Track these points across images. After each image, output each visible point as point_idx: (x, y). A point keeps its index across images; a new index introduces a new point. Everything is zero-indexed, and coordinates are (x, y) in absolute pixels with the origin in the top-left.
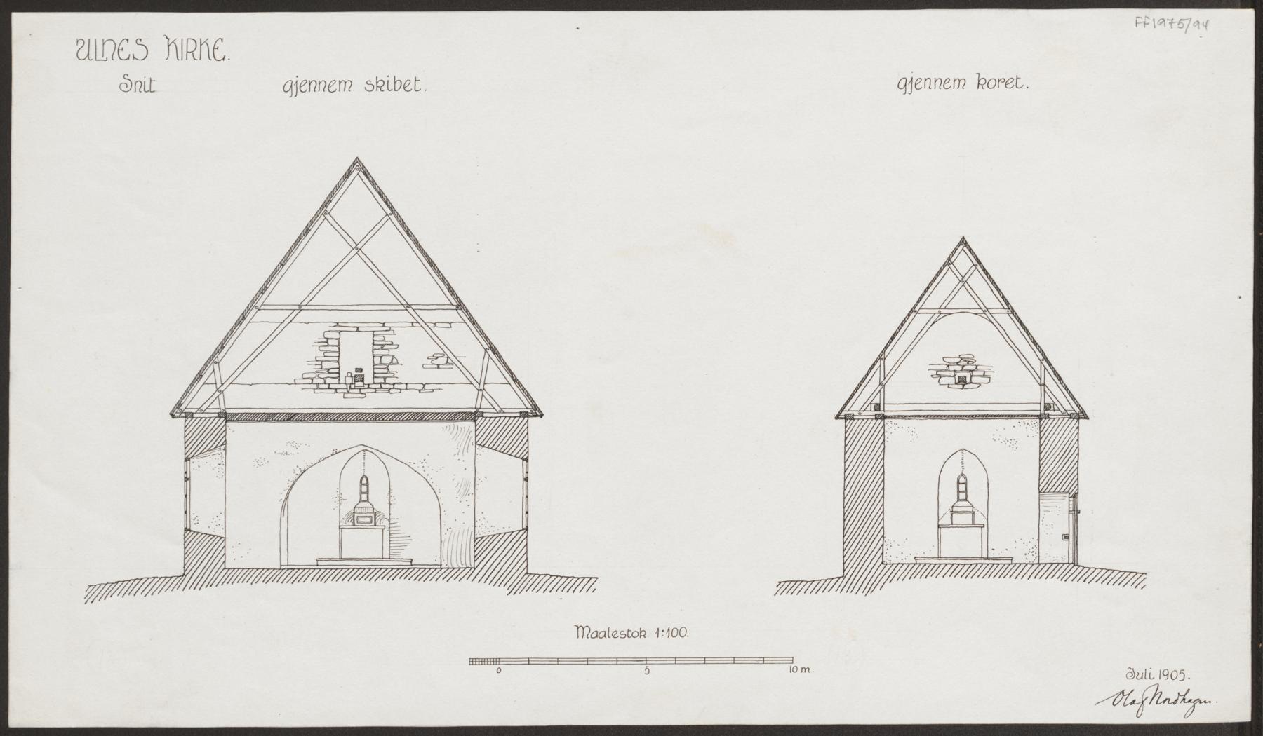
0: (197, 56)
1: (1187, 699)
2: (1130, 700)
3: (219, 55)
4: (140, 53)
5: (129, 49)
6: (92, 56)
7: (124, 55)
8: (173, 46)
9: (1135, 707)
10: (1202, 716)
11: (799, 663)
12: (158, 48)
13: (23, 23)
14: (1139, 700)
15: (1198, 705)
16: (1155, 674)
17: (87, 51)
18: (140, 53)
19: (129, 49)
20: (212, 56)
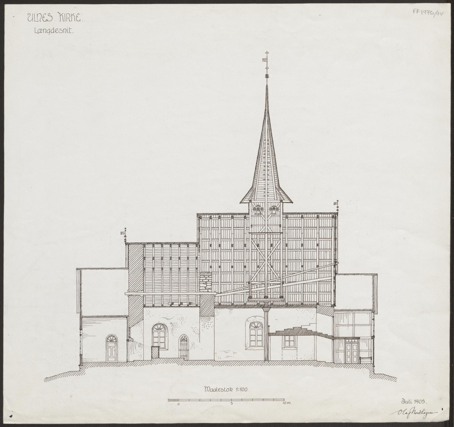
0: (71, 20)
2: (405, 412)
3: (78, 19)
4: (49, 18)
5: (46, 17)
7: (45, 19)
8: (61, 16)
10: (430, 419)
11: (286, 401)
12: (56, 17)
13: (9, 9)
14: (408, 413)
15: (428, 414)
17: (32, 18)
18: (49, 18)
19: (46, 17)
20: (76, 20)
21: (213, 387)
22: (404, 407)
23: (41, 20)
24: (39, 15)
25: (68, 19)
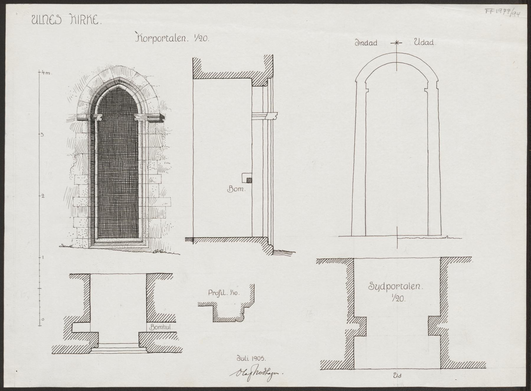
0: (86, 22)
1: (268, 372)
3: (96, 22)
4: (58, 21)
6: (38, 22)
7: (52, 22)
8: (74, 18)
9: (247, 376)
12: (67, 19)
15: (273, 375)
16: (250, 358)
17: (37, 21)
18: (58, 21)
21: (378, 282)
22: (243, 365)
23: (48, 22)
24: (46, 17)
25: (82, 21)
